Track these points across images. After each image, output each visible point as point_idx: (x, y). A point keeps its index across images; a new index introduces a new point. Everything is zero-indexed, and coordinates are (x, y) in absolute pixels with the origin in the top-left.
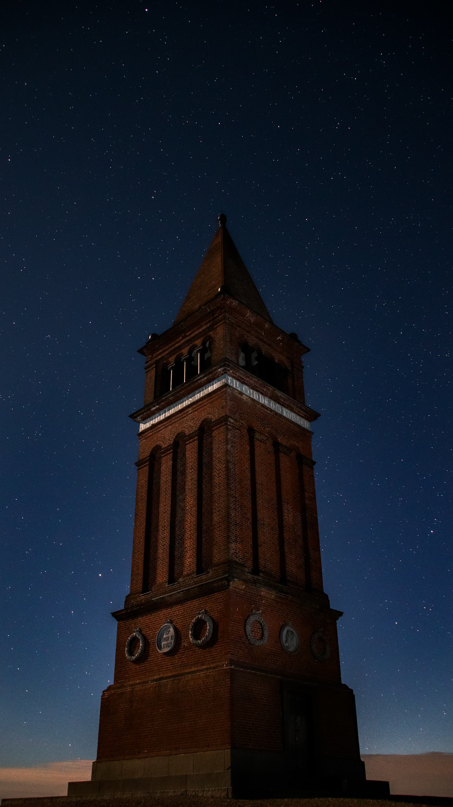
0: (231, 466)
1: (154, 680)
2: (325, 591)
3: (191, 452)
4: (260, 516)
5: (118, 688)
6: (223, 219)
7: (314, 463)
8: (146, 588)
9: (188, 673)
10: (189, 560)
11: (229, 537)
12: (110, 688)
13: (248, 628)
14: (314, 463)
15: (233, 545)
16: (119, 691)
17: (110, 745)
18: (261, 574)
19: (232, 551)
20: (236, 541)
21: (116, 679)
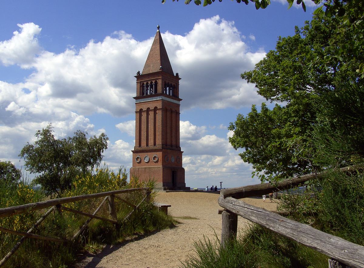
3: (151, 114)
8: (140, 145)
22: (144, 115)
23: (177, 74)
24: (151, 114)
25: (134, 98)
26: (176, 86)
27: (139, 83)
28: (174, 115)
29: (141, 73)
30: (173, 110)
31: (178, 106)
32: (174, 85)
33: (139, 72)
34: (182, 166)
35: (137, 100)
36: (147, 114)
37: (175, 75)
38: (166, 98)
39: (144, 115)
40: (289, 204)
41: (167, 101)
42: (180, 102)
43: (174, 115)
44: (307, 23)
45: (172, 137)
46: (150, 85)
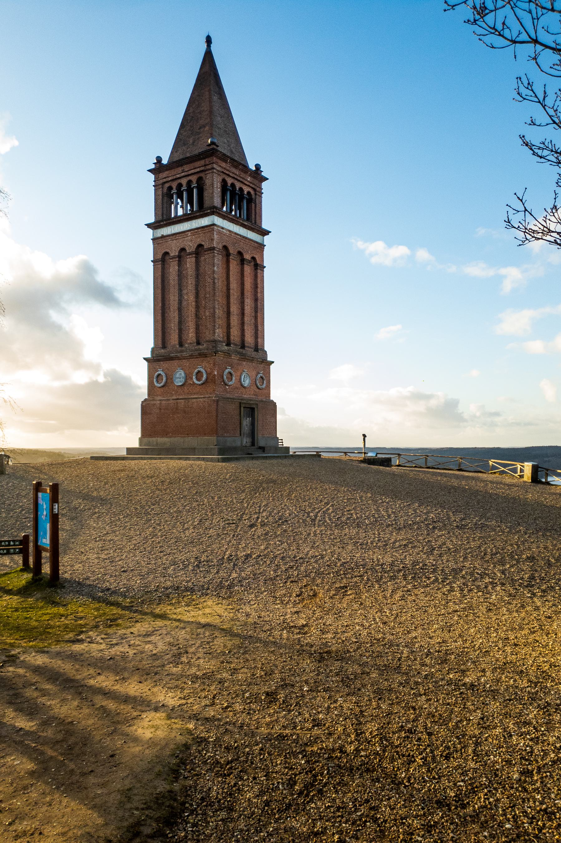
0: (216, 281)
1: (173, 400)
2: (265, 349)
3: (190, 262)
4: (231, 310)
5: (151, 401)
6: (209, 40)
7: (265, 267)
8: (164, 346)
9: (194, 398)
10: (191, 335)
11: (215, 326)
12: (146, 400)
13: (225, 377)
14: (265, 267)
15: (217, 331)
16: (152, 402)
17: (148, 430)
18: (232, 345)
19: (217, 334)
20: (219, 328)
21: (149, 394)
22: (173, 268)
23: (258, 167)
24: (190, 262)
25: (149, 226)
26: (253, 196)
27: (161, 186)
28: (248, 269)
29: (165, 161)
30: (247, 257)
31: (261, 246)
32: (249, 193)
33: (159, 159)
34: (269, 397)
35: (155, 231)
36: (179, 265)
37: (254, 169)
38: (225, 221)
39: (173, 268)
40: (227, 811)
41: (230, 231)
42: (266, 237)
43: (248, 269)
44: (556, 93)
45: (243, 324)
46: (186, 190)
